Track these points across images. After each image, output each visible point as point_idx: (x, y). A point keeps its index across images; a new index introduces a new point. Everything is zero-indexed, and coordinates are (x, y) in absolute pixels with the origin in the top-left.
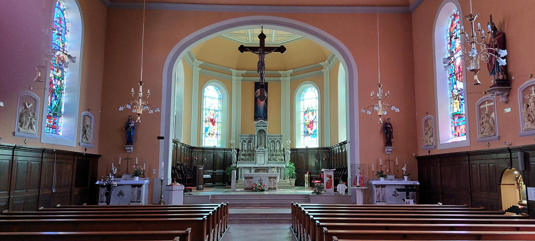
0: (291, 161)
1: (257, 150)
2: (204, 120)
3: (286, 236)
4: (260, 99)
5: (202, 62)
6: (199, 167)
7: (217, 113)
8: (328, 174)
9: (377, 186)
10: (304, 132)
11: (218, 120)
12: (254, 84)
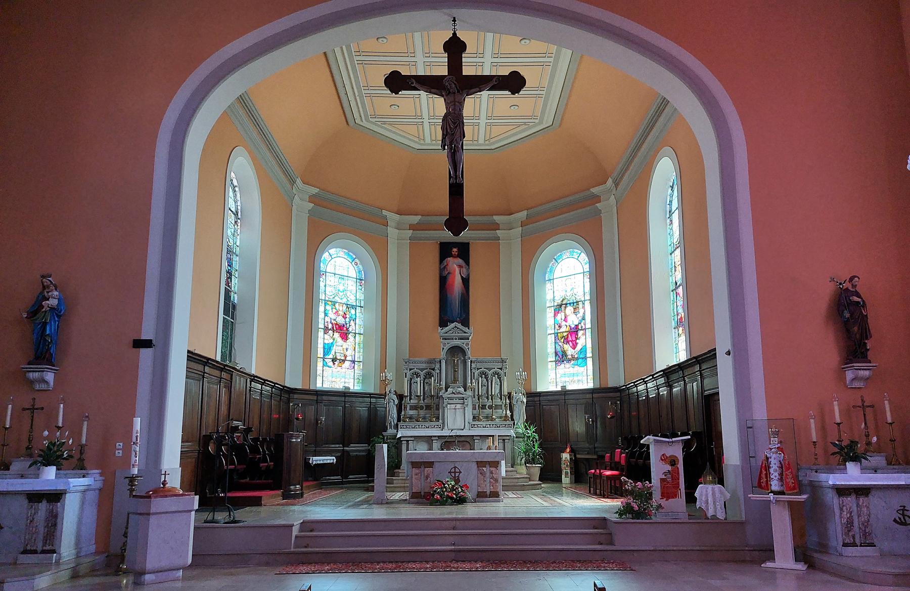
0: (531, 419)
1: (445, 395)
2: (321, 326)
4: (455, 251)
5: (315, 191)
6: (292, 436)
7: (353, 311)
8: (663, 453)
9: (842, 491)
10: (556, 354)
11: (358, 326)
12: (438, 247)
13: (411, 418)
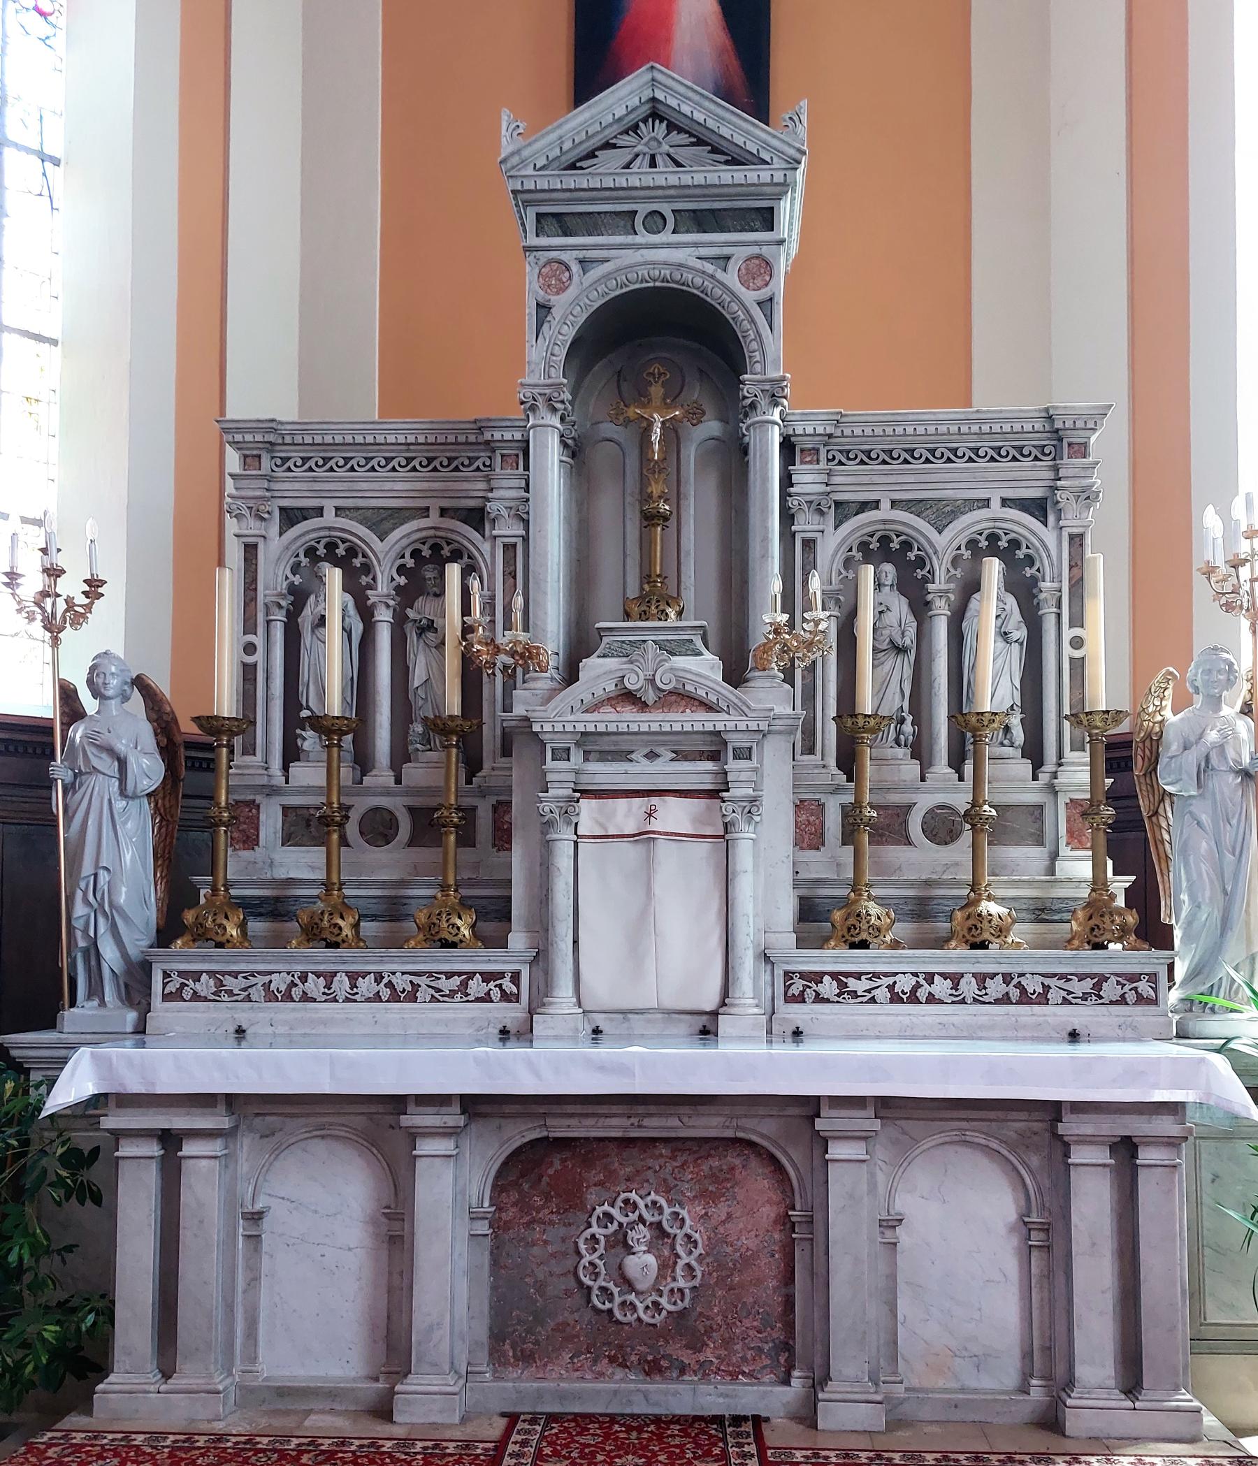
1: (557, 713)
3: (775, 1283)
12: (797, 901)
13: (274, 908)
